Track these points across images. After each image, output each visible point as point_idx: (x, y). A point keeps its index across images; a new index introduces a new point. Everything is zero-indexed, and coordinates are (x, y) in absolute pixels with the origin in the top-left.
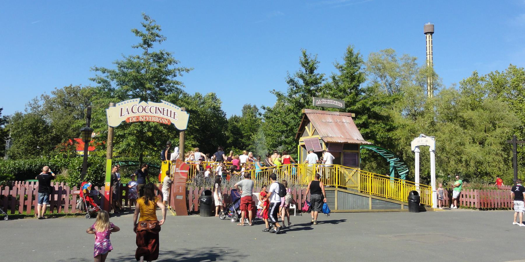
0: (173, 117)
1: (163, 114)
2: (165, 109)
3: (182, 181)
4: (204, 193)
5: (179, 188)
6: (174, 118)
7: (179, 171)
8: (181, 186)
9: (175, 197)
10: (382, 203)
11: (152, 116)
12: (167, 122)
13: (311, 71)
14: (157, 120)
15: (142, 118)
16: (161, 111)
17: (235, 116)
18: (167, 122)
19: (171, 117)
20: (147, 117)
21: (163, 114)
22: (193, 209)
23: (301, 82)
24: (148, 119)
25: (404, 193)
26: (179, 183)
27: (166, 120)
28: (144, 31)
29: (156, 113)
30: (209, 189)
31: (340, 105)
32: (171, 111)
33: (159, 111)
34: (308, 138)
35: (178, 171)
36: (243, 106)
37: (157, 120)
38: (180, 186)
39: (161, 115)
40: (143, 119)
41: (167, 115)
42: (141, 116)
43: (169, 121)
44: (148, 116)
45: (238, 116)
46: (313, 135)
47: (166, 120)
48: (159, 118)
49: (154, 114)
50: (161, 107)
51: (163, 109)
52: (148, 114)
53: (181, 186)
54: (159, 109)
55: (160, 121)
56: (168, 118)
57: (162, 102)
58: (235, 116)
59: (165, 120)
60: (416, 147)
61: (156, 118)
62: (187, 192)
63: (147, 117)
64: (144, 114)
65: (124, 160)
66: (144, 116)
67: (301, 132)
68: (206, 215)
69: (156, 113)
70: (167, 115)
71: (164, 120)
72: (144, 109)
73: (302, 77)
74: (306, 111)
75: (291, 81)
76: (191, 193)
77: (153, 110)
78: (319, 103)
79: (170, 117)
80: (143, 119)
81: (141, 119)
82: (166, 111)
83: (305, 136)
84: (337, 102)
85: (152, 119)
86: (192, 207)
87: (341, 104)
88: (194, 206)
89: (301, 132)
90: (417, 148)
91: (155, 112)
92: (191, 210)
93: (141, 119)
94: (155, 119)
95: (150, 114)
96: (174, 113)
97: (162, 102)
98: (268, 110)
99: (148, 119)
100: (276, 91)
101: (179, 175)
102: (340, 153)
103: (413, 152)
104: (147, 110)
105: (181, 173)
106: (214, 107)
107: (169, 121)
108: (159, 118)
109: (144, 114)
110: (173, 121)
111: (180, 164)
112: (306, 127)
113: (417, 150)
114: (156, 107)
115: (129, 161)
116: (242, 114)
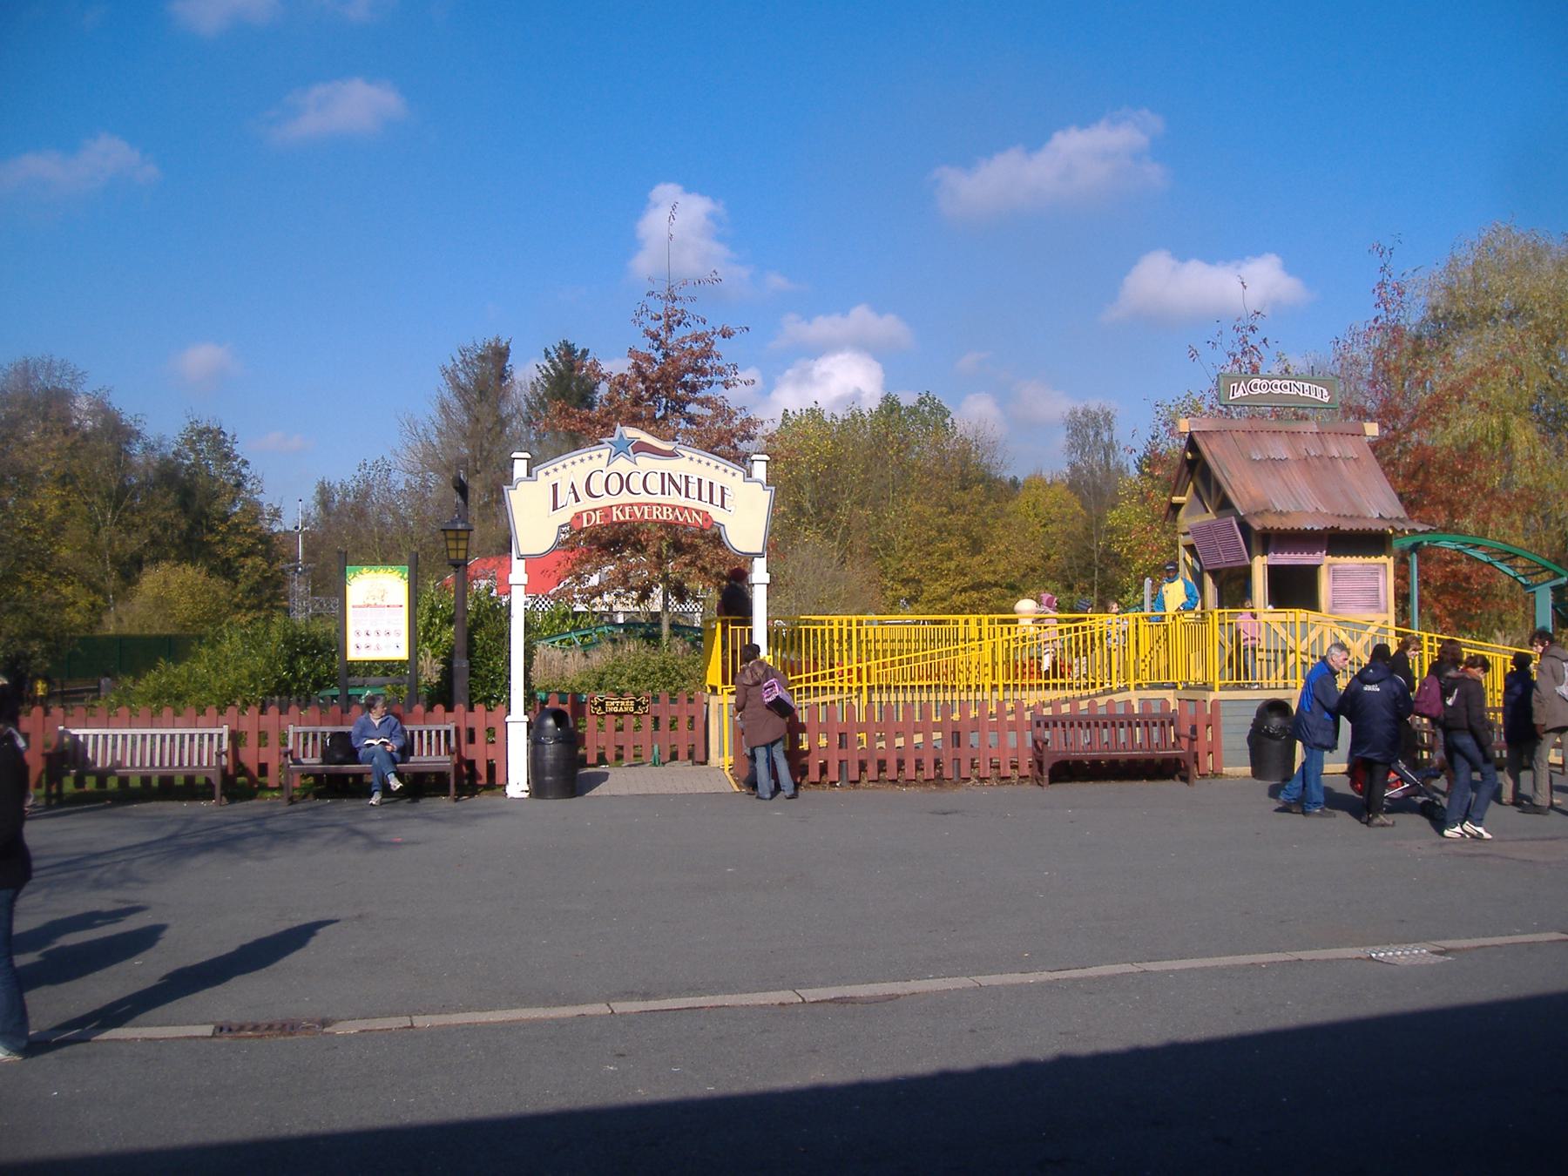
2: (690, 479)
6: (723, 506)
14: (668, 516)
16: (678, 483)
24: (639, 515)
29: (663, 493)
31: (1319, 397)
32: (711, 484)
33: (672, 487)
37: (668, 516)
39: (681, 500)
41: (700, 499)
42: (618, 506)
49: (659, 499)
51: (687, 477)
59: (694, 514)
69: (663, 493)
77: (654, 483)
82: (696, 485)
87: (1325, 393)
91: (659, 491)
95: (644, 498)
96: (722, 488)
104: (635, 483)
108: (674, 510)
109: (626, 498)
110: (717, 515)
114: (663, 474)
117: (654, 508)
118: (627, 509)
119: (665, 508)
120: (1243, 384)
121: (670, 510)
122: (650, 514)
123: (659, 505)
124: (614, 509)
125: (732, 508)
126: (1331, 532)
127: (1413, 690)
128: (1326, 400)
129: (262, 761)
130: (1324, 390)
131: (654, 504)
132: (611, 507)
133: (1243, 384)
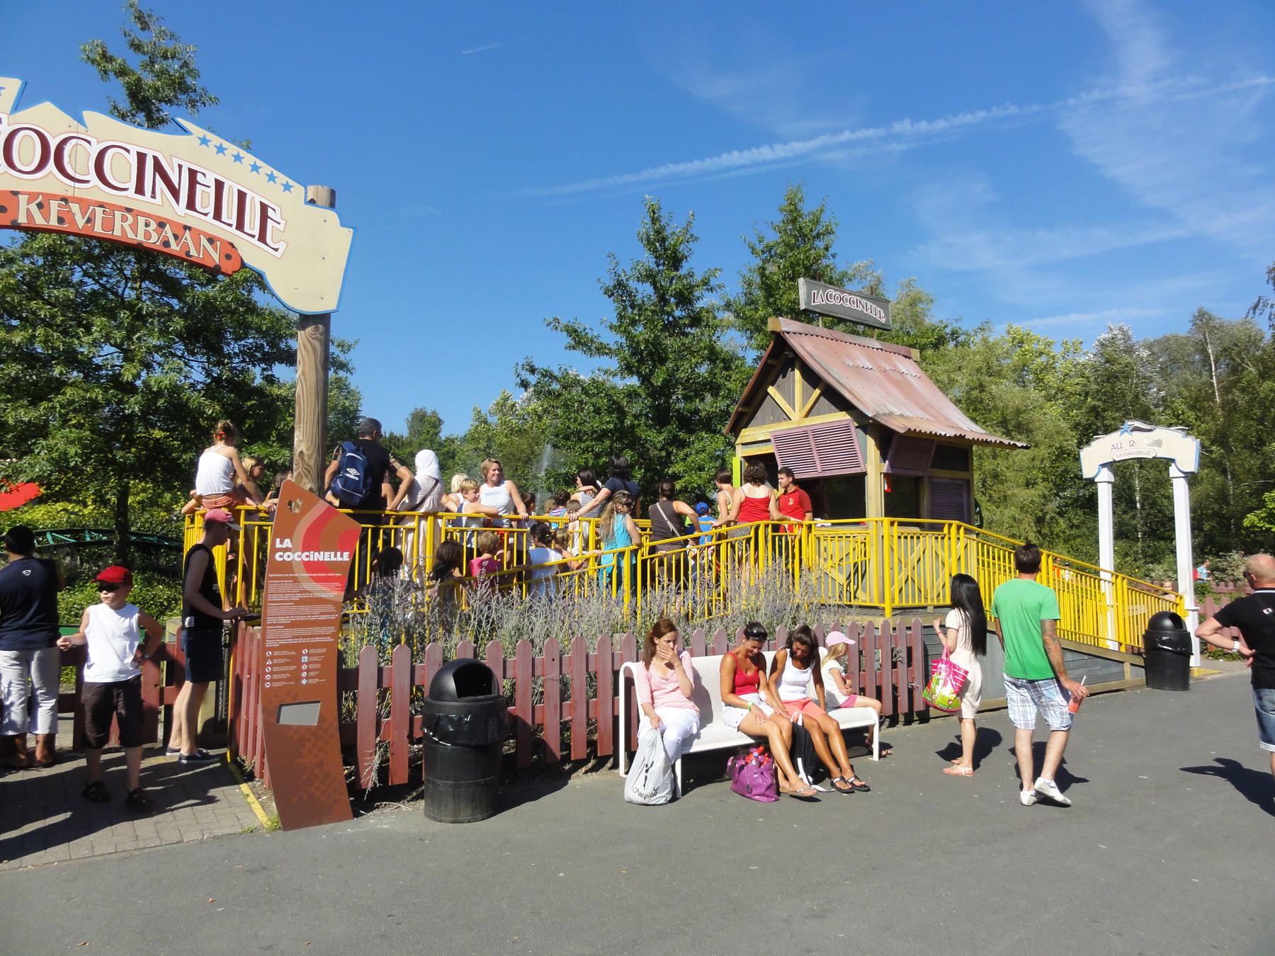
0: (256, 232)
1: (191, 205)
2: (200, 178)
3: (315, 613)
4: (451, 684)
5: (296, 660)
6: (262, 238)
7: (297, 557)
8: (308, 646)
9: (273, 714)
10: (1080, 663)
11: (114, 207)
12: (216, 257)
13: (675, 261)
14: (148, 236)
15: (33, 208)
16: (175, 182)
17: (392, 434)
18: (216, 257)
19: (240, 226)
20: (75, 207)
21: (191, 205)
22: (383, 772)
23: (645, 291)
24: (81, 222)
25: (1079, 624)
26: (301, 631)
27: (211, 240)
28: (135, 62)
29: (140, 190)
30: (470, 655)
31: (877, 317)
32: (242, 196)
33: (160, 183)
34: (783, 427)
35: (288, 557)
36: (412, 410)
37: (148, 236)
38: (298, 648)
39: (179, 211)
40: (47, 218)
41: (218, 215)
42: (32, 196)
43: (229, 250)
44: (80, 201)
45: (397, 433)
46: (807, 415)
47: (211, 240)
48: (162, 225)
49: (129, 197)
50: (176, 162)
51: (193, 174)
52: (79, 191)
53: (308, 646)
54: (158, 167)
55: (166, 244)
56: (226, 232)
57: (185, 131)
58: (392, 434)
59: (204, 241)
60: (1103, 465)
61: (142, 220)
62: (347, 679)
63: (75, 207)
64: (51, 182)
65: (65, 527)
66: (54, 197)
67: (746, 410)
68: (465, 813)
69: (140, 190)
70: (218, 215)
71: (198, 245)
72: (53, 155)
73: (651, 277)
74: (782, 324)
75: (619, 289)
76: (367, 684)
77: (121, 169)
78: (818, 301)
79: (233, 229)
80: (47, 218)
81: (29, 212)
82: (212, 191)
83: (764, 423)
84: (869, 304)
85: (108, 223)
86: (376, 760)
87: (883, 315)
88: (385, 761)
89: (746, 410)
90: (1105, 470)
91: (132, 185)
92: (370, 779)
93: (29, 212)
94: (134, 227)
95: (94, 190)
96: (264, 208)
97: (185, 131)
98: (543, 376)
99: (81, 222)
100: (564, 322)
101: (296, 580)
102: (917, 481)
103: (1091, 482)
104: (80, 159)
105: (310, 566)
106: (344, 408)
107: (230, 251)
108: (162, 225)
109: (51, 182)
110: (252, 254)
111: (303, 513)
112: (771, 390)
113: (1106, 476)
114: (141, 158)
115: (83, 531)
116: (407, 430)
117: (118, 214)
118: (54, 206)
119: (142, 220)
120: (821, 292)
121: (153, 225)
122: (108, 223)
123: (129, 210)
124: (23, 199)
125: (282, 246)
126: (919, 436)
127: (121, 720)
128: (883, 321)
129: (878, 684)
130: (882, 311)
131: (120, 208)
132: (15, 193)
133: (821, 292)
